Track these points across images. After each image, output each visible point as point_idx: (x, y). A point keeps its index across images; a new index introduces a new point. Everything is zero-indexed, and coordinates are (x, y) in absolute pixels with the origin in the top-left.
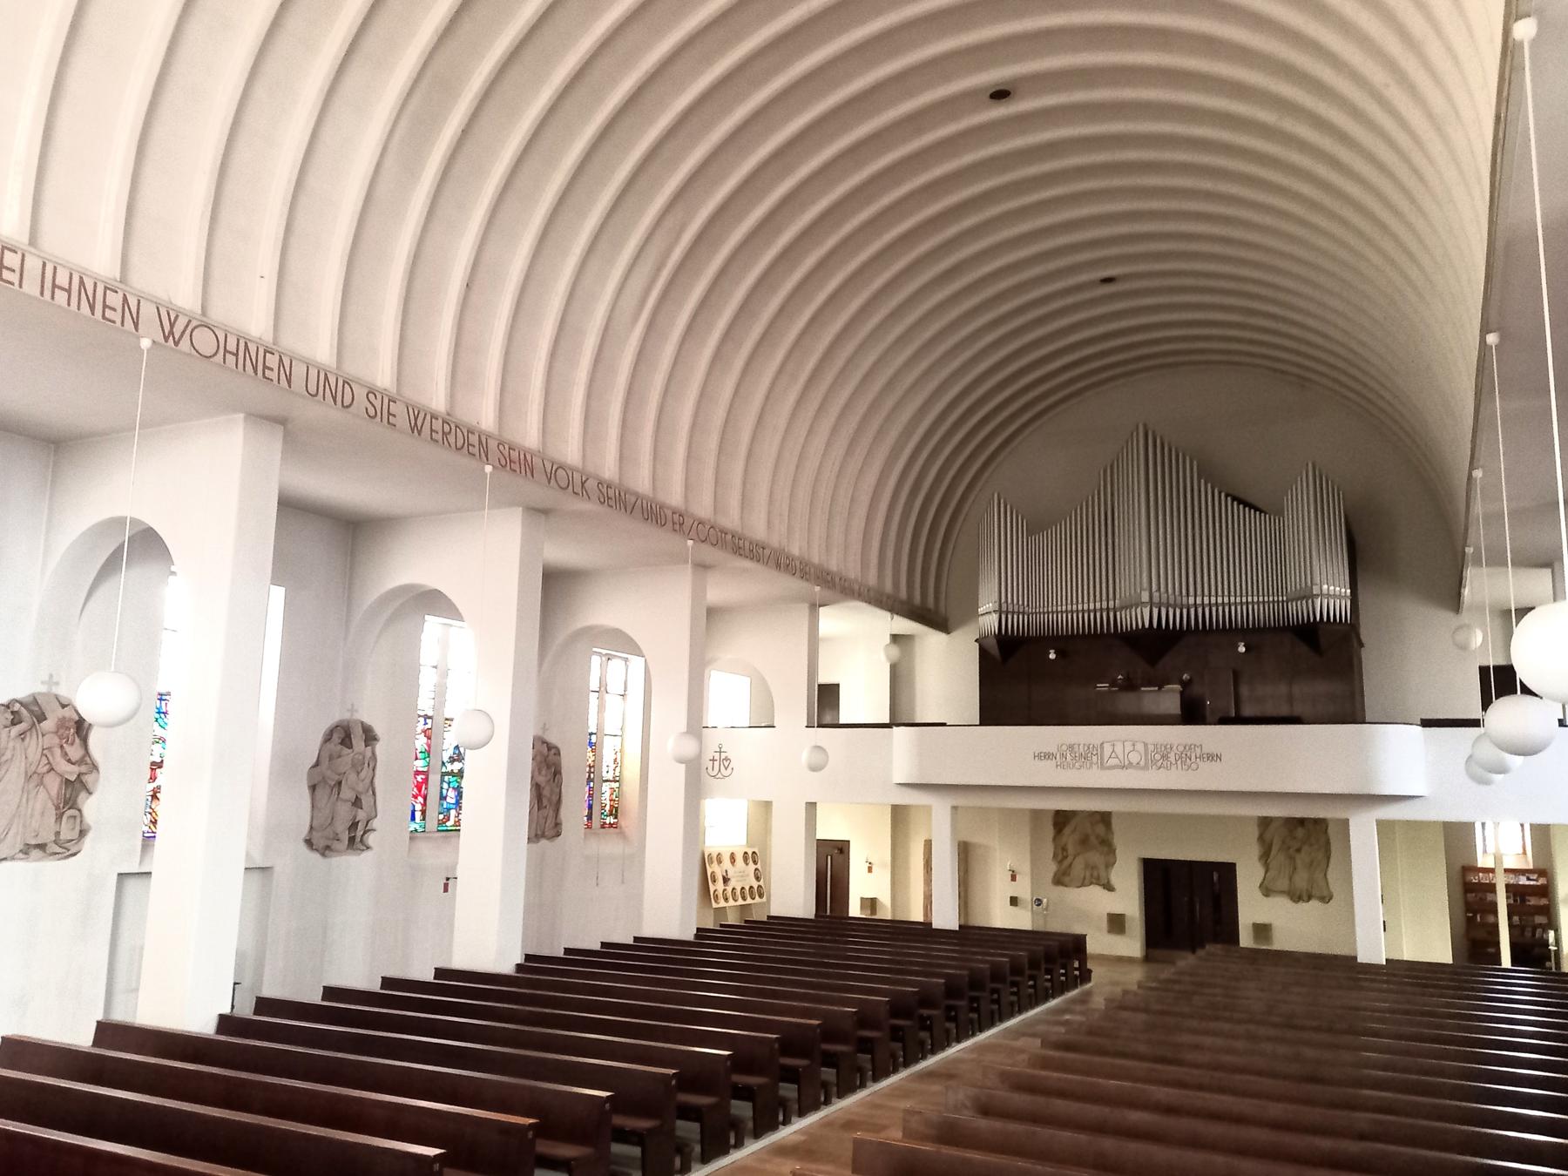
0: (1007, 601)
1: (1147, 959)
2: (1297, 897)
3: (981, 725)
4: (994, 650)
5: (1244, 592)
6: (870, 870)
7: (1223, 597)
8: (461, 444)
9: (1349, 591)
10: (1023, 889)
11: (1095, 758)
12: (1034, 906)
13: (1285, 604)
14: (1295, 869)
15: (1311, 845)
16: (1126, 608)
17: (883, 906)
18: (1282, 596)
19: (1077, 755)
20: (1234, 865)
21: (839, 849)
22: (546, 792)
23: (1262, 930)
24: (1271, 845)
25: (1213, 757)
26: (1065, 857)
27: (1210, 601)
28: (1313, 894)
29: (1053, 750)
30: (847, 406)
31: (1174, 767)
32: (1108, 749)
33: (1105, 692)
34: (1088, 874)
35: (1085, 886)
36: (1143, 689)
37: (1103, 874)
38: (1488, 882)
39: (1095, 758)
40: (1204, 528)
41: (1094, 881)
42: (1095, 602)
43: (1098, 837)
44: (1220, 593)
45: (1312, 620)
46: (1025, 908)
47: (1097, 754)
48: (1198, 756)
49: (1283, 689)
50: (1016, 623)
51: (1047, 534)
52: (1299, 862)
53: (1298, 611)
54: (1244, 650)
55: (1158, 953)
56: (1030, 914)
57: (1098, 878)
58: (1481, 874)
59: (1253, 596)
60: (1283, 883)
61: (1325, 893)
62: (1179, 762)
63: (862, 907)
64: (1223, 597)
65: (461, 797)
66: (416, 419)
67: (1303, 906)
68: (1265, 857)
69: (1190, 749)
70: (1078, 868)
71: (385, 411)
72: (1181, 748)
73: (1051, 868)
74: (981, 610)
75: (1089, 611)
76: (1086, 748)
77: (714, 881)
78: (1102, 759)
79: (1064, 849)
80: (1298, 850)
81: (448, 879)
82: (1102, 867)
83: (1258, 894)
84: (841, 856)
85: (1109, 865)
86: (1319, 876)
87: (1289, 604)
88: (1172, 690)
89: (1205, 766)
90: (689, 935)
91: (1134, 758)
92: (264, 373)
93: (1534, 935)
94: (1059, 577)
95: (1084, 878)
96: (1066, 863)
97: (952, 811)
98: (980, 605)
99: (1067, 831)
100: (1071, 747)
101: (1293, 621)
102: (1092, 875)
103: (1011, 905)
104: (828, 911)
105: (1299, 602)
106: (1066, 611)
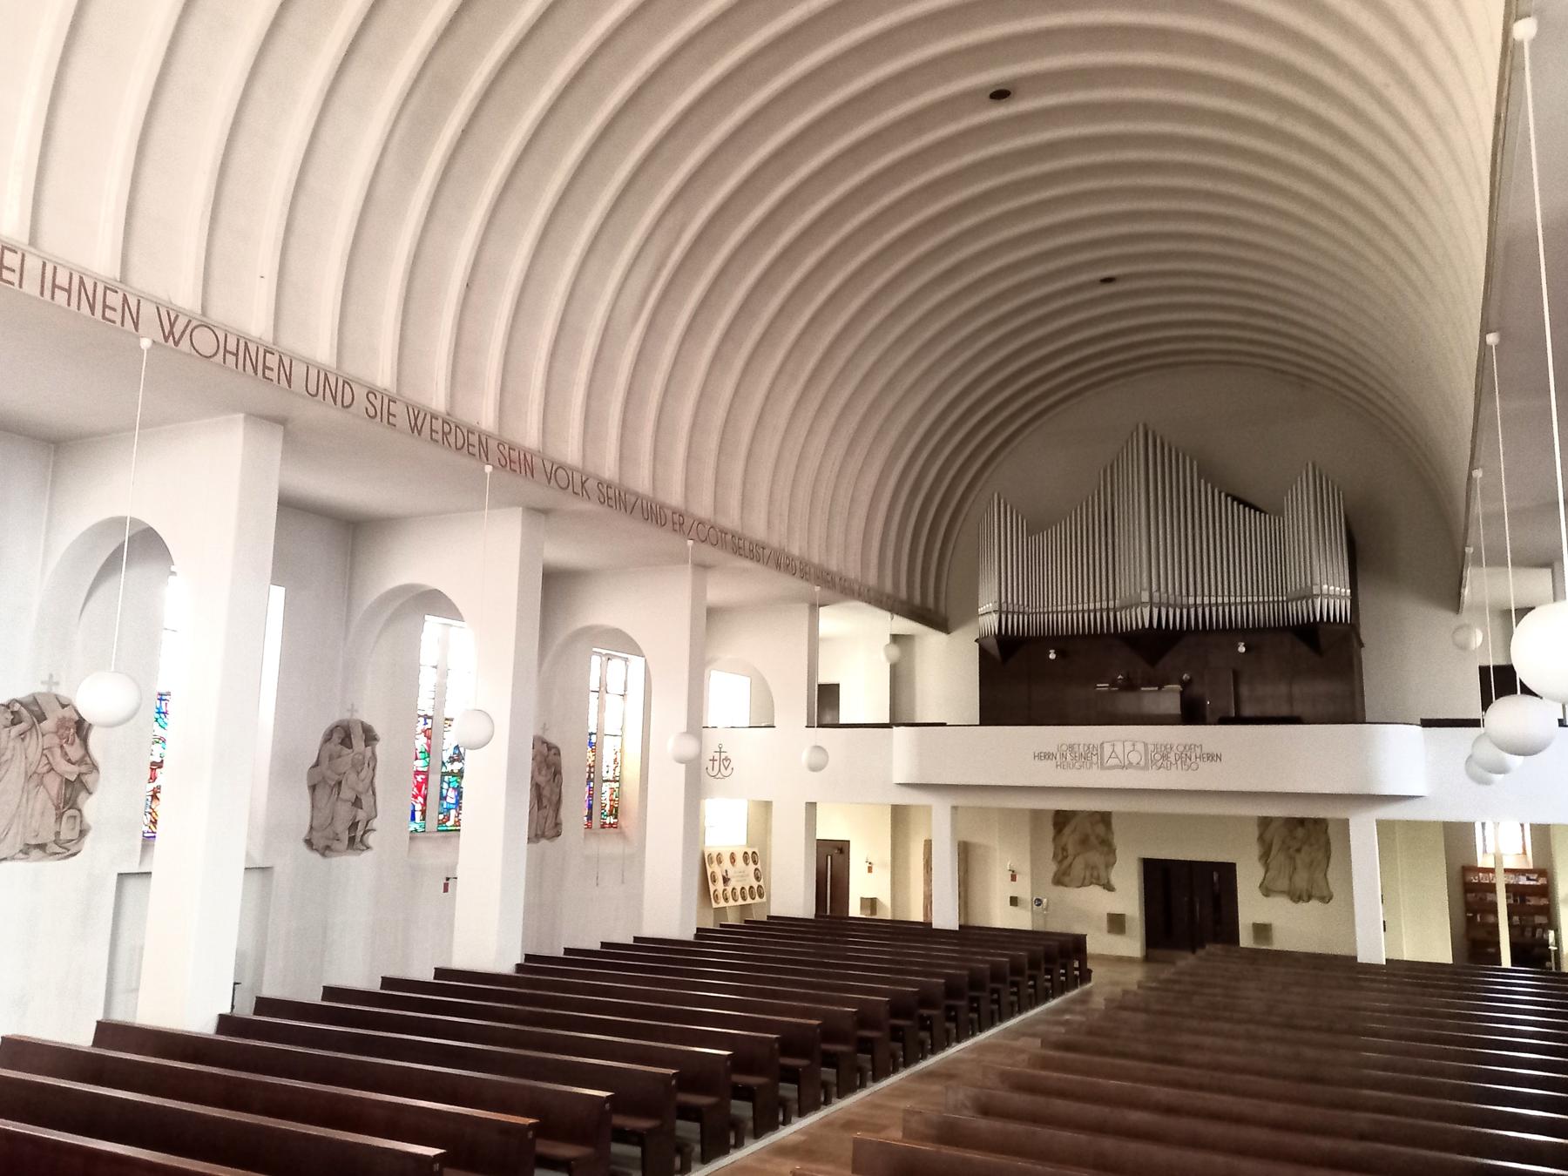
0: (1007, 601)
1: (1147, 959)
2: (1297, 897)
3: (981, 725)
4: (994, 650)
5: (1244, 592)
6: (870, 870)
7: (1223, 597)
8: (461, 444)
9: (1349, 591)
10: (1023, 889)
11: (1095, 758)
12: (1034, 906)
13: (1285, 604)
14: (1295, 869)
15: (1311, 845)
16: (1126, 608)
17: (883, 906)
18: (1282, 596)
19: (1077, 755)
20: (1234, 865)
21: (839, 849)
22: (546, 792)
23: (1262, 930)
24: (1271, 845)
25: (1213, 757)
26: (1065, 857)
27: (1210, 601)
28: (1313, 894)
29: (1053, 750)
30: (847, 406)
31: (1174, 767)
32: (1108, 749)
33: (1105, 692)
34: (1088, 874)
35: (1085, 886)
36: (1143, 689)
37: (1103, 874)
38: (1488, 882)
39: (1095, 758)
40: (1204, 528)
41: (1094, 881)
42: (1095, 602)
43: (1098, 837)
44: (1220, 593)
45: (1312, 620)
46: (1025, 908)
47: (1097, 754)
48: (1198, 756)
49: (1283, 689)
50: (1016, 623)
51: (1047, 534)
52: (1299, 862)
53: (1298, 611)
54: (1244, 650)
55: (1158, 953)
56: (1030, 914)
57: (1098, 878)
58: (1481, 874)
59: (1253, 596)
60: (1283, 883)
61: (1325, 893)
62: (1179, 762)
63: (862, 907)
64: (1223, 597)
65: (461, 797)
66: (416, 419)
67: (1303, 906)
68: (1265, 857)
69: (1190, 749)
70: (1078, 868)
71: (385, 411)
72: (1181, 748)
73: (1051, 868)
74: (981, 610)
75: (1089, 611)
76: (1086, 748)
77: (714, 881)
78: (1102, 759)
79: (1064, 849)
80: (1298, 850)
81: (448, 879)
82: (1102, 867)
83: (1258, 894)
84: (841, 856)
85: (1109, 865)
86: (1319, 876)
87: (1289, 604)
88: (1172, 690)
89: (1205, 766)
90: (689, 935)
91: (1134, 758)
92: (264, 373)
93: (1534, 935)
94: (1059, 577)
95: (1084, 878)
96: (1066, 863)
97: (952, 811)
98: (980, 605)
99: (1067, 831)
100: (1071, 747)
101: (1293, 621)
102: (1092, 875)
103: (1011, 905)
104: (828, 911)
105: (1299, 602)
106: (1066, 611)
